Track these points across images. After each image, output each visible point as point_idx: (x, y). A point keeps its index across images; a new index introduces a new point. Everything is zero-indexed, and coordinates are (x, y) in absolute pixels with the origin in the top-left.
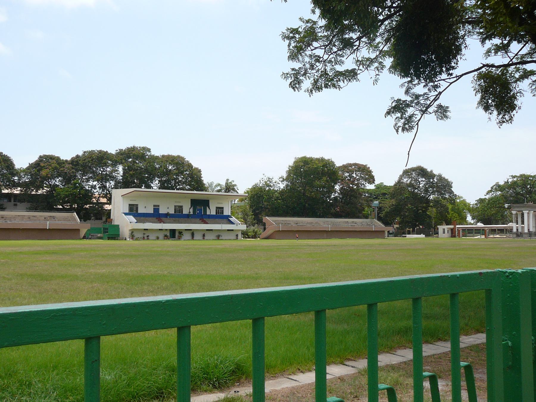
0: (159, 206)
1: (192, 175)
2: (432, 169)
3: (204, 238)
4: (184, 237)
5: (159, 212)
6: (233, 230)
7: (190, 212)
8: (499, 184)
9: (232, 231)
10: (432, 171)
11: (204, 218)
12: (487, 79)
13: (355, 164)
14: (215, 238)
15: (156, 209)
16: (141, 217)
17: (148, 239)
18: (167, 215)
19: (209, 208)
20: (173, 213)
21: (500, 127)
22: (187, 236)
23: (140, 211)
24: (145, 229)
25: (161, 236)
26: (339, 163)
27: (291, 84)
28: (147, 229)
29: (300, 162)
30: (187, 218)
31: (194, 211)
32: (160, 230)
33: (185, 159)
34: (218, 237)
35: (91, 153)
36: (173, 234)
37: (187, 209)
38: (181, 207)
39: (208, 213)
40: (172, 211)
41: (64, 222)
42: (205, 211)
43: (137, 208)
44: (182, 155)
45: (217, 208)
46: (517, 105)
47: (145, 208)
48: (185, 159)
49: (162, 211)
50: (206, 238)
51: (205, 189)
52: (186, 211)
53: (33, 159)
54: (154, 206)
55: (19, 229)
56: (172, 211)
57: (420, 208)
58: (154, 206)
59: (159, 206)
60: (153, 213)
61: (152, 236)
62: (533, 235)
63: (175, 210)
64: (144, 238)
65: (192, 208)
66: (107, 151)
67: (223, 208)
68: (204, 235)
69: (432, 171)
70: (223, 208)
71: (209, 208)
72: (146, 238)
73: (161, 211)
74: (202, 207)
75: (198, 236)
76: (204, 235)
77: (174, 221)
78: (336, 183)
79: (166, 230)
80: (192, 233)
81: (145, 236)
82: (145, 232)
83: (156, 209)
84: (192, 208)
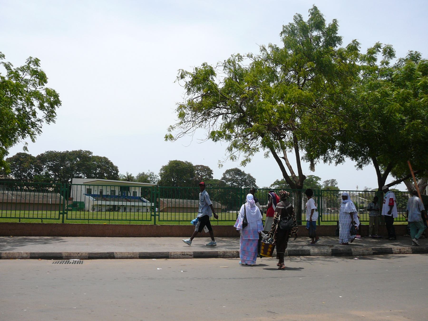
2: (244, 170)
8: (279, 180)
10: (244, 172)
11: (128, 199)
13: (202, 166)
15: (101, 192)
16: (101, 196)
26: (194, 165)
29: (173, 164)
30: (118, 198)
31: (122, 194)
33: (213, 174)
35: (52, 152)
40: (109, 193)
46: (282, 39)
48: (213, 174)
51: (118, 179)
52: (117, 194)
57: (243, 197)
60: (403, 182)
66: (67, 151)
69: (244, 172)
73: (104, 193)
74: (126, 191)
78: (68, 167)
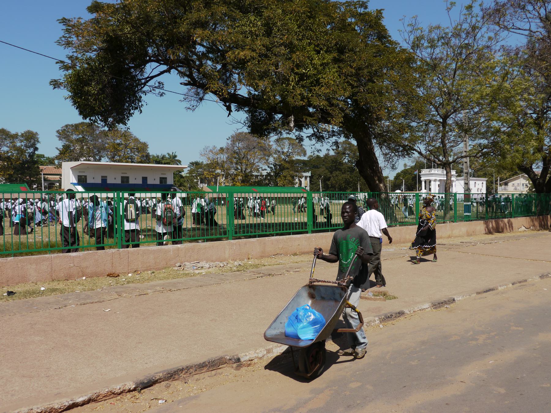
0: (106, 177)
5: (106, 182)
12: (33, 154)
15: (104, 179)
20: (120, 183)
23: (90, 181)
27: (197, 164)
38: (86, 176)
40: (119, 181)
41: (61, 211)
43: (86, 179)
47: (94, 179)
49: (150, 182)
53: (394, 178)
58: (102, 177)
59: (106, 177)
62: (333, 307)
63: (160, 181)
67: (166, 178)
70: (166, 178)
83: (104, 179)
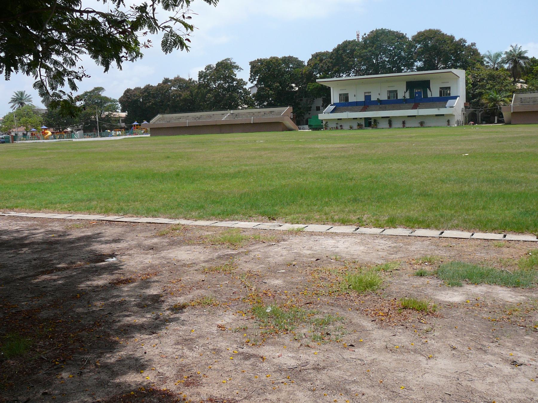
1: (21, 99)
3: (404, 126)
4: (380, 125)
6: (443, 115)
7: (404, 97)
9: (442, 117)
14: (419, 125)
15: (368, 97)
17: (342, 129)
18: (357, 104)
19: (430, 90)
20: (439, 96)
21: (90, 77)
22: (385, 124)
24: (338, 119)
25: (355, 126)
28: (341, 119)
32: (354, 119)
34: (422, 124)
36: (369, 123)
37: (402, 93)
39: (429, 96)
42: (426, 94)
44: (434, 26)
45: (441, 88)
50: (407, 125)
52: (400, 97)
54: (365, 93)
55: (186, 127)
56: (384, 97)
61: (346, 126)
63: (441, 92)
64: (337, 128)
65: (408, 91)
68: (404, 123)
71: (430, 90)
72: (339, 128)
75: (395, 124)
76: (404, 123)
77: (380, 108)
79: (361, 118)
80: (390, 121)
81: (339, 126)
82: (339, 122)
83: (368, 97)
84: (408, 91)
